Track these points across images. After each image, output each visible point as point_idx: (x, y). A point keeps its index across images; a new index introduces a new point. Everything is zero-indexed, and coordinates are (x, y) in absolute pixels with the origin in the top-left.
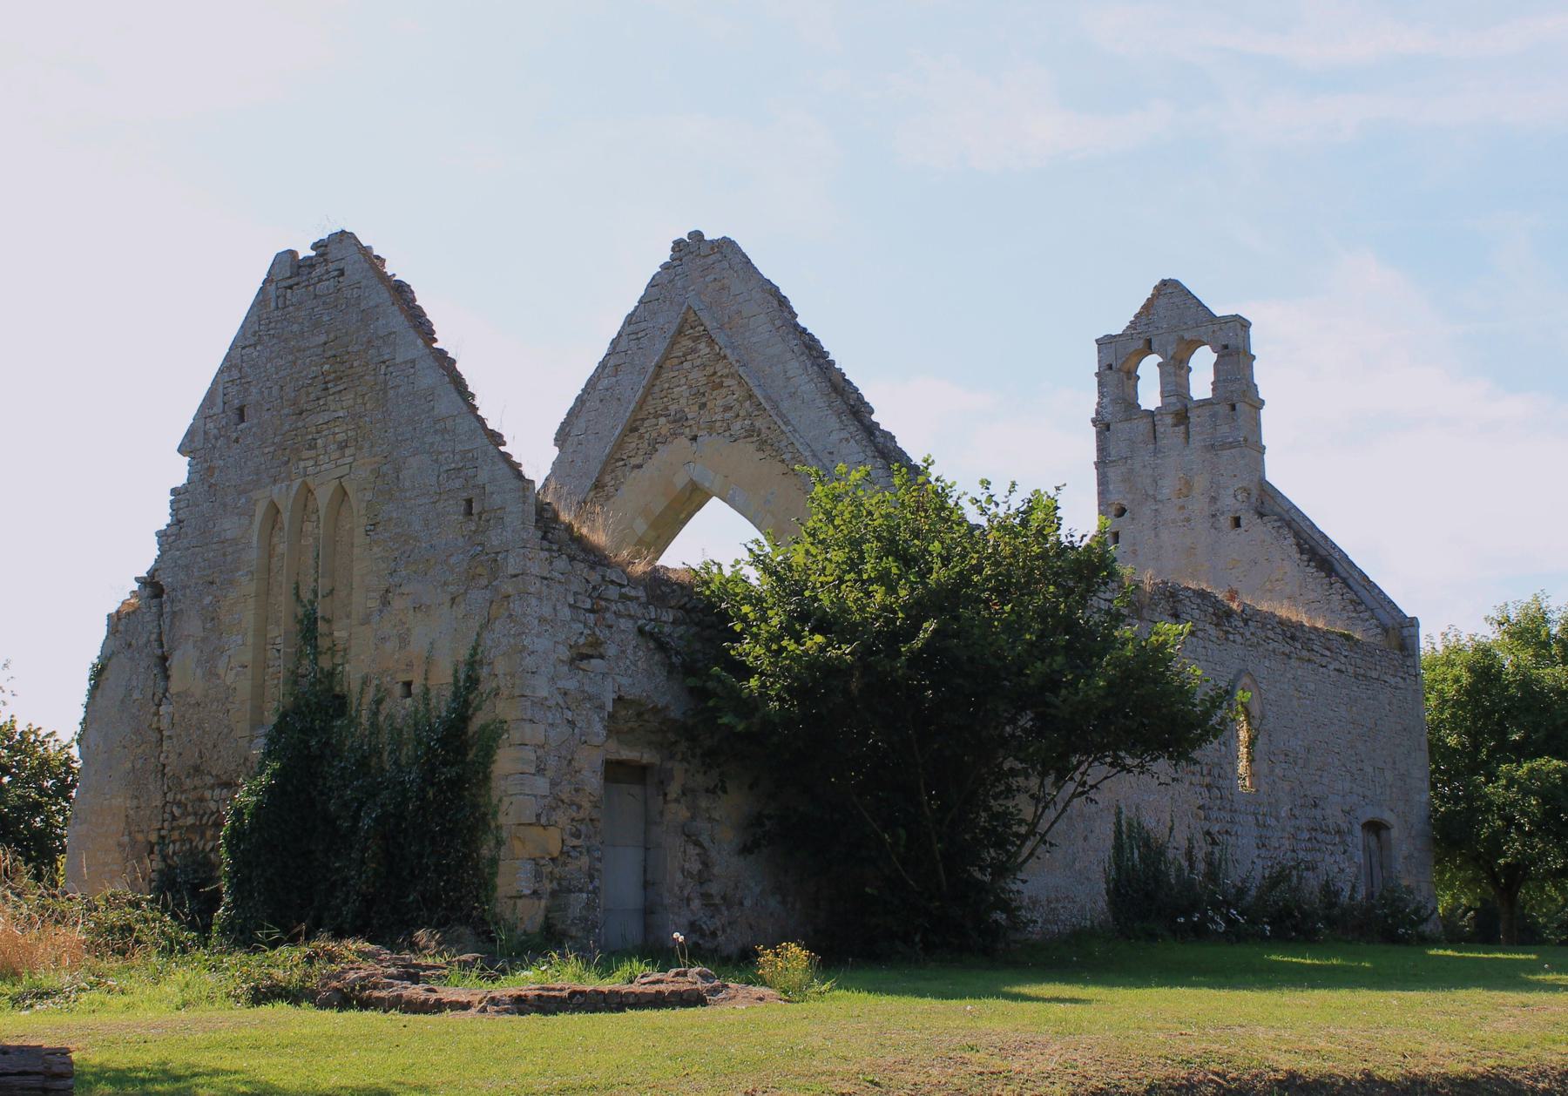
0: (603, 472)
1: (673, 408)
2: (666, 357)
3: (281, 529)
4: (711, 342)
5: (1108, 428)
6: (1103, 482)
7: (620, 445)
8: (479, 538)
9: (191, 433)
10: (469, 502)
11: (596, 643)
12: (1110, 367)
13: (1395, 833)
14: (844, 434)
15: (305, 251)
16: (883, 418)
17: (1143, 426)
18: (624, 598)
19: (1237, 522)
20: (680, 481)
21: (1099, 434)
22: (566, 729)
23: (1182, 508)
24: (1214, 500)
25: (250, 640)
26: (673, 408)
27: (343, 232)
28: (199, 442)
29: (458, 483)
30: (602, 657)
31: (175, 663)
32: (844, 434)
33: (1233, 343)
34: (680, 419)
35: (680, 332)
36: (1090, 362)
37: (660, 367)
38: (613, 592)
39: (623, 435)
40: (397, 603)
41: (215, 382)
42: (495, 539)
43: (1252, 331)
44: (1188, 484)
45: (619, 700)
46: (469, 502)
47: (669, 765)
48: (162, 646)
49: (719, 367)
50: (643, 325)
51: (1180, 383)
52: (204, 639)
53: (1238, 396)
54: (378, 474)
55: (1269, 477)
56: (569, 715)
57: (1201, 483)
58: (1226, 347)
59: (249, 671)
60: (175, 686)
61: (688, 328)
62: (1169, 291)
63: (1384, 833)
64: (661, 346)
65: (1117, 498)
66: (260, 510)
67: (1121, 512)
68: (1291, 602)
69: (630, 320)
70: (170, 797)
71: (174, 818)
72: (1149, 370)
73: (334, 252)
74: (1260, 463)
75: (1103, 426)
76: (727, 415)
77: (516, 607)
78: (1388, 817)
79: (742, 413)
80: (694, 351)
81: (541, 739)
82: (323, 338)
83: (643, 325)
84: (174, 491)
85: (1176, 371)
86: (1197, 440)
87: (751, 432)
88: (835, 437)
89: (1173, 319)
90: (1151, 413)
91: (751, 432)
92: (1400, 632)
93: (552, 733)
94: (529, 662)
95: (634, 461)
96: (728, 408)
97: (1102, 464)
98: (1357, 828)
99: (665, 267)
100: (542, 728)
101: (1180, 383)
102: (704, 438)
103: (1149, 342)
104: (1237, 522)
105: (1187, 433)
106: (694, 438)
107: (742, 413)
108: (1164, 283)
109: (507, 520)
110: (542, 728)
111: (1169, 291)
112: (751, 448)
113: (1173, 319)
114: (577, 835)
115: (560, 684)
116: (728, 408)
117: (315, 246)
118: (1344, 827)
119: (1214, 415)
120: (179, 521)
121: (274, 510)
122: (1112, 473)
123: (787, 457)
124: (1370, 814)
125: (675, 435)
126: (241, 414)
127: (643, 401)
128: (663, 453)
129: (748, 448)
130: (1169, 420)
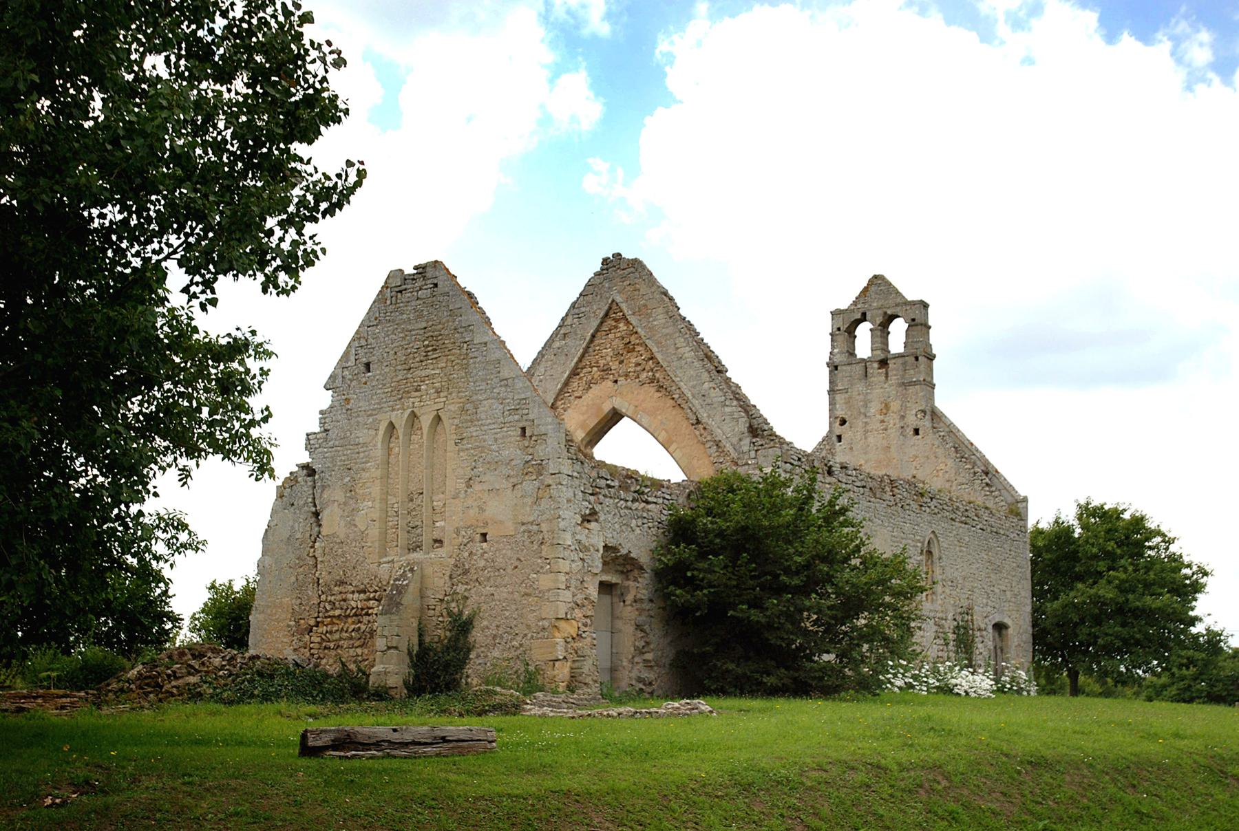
0: (556, 400)
1: (602, 362)
2: (597, 331)
3: (398, 438)
4: (628, 323)
5: (836, 368)
6: (832, 403)
7: (566, 384)
8: (531, 450)
9: (333, 377)
10: (523, 429)
11: (594, 513)
12: (839, 329)
13: (1010, 631)
14: (712, 385)
15: (409, 270)
16: (734, 374)
17: (859, 369)
18: (609, 486)
19: (916, 432)
20: (607, 408)
21: (831, 372)
22: (580, 563)
23: (883, 421)
24: (903, 417)
25: (377, 505)
26: (602, 362)
27: (436, 262)
28: (339, 382)
29: (516, 417)
30: (596, 521)
31: (324, 516)
32: (712, 385)
33: (919, 325)
34: (606, 370)
35: (606, 315)
36: (826, 326)
37: (593, 336)
38: (602, 483)
39: (569, 377)
40: (477, 487)
41: (349, 346)
42: (541, 451)
43: (930, 309)
44: (887, 406)
45: (606, 547)
46: (523, 429)
47: (627, 583)
48: (315, 506)
49: (633, 338)
50: (583, 309)
51: (882, 340)
52: (345, 504)
53: (920, 353)
54: (463, 410)
55: (937, 404)
56: (581, 555)
57: (895, 406)
58: (913, 320)
59: (377, 523)
60: (324, 531)
61: (611, 313)
62: (878, 284)
63: (1004, 632)
64: (595, 324)
65: (840, 413)
66: (383, 427)
67: (843, 422)
68: (938, 474)
69: (573, 305)
70: (323, 597)
71: (327, 611)
72: (864, 332)
73: (430, 273)
74: (931, 397)
75: (833, 367)
76: (639, 368)
77: (554, 492)
78: (1007, 621)
79: (647, 368)
80: (616, 327)
81: (567, 570)
82: (424, 325)
83: (583, 309)
84: (321, 412)
85: (882, 330)
86: (893, 379)
87: (652, 380)
88: (706, 385)
89: (879, 303)
90: (863, 360)
91: (652, 380)
92: (1017, 508)
93: (574, 565)
94: (562, 524)
95: (576, 394)
96: (638, 365)
97: (832, 392)
98: (990, 627)
99: (597, 274)
100: (568, 562)
101: (882, 340)
102: (622, 380)
103: (864, 314)
104: (916, 432)
105: (887, 374)
106: (616, 382)
107: (647, 368)
108: (875, 277)
109: (549, 441)
110: (568, 562)
111: (878, 284)
112: (653, 390)
113: (879, 303)
114: (585, 625)
115: (578, 537)
116: (638, 365)
117: (416, 268)
118: (983, 626)
119: (904, 364)
120: (326, 430)
121: (392, 426)
122: (838, 397)
123: (676, 396)
124: (997, 618)
125: (603, 379)
126: (368, 366)
127: (583, 356)
128: (595, 390)
129: (651, 390)
130: (876, 365)
